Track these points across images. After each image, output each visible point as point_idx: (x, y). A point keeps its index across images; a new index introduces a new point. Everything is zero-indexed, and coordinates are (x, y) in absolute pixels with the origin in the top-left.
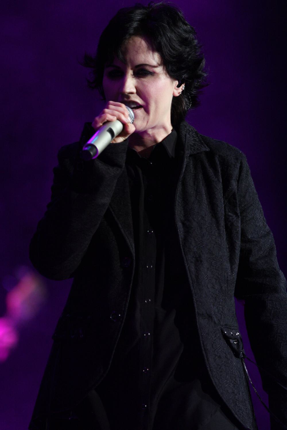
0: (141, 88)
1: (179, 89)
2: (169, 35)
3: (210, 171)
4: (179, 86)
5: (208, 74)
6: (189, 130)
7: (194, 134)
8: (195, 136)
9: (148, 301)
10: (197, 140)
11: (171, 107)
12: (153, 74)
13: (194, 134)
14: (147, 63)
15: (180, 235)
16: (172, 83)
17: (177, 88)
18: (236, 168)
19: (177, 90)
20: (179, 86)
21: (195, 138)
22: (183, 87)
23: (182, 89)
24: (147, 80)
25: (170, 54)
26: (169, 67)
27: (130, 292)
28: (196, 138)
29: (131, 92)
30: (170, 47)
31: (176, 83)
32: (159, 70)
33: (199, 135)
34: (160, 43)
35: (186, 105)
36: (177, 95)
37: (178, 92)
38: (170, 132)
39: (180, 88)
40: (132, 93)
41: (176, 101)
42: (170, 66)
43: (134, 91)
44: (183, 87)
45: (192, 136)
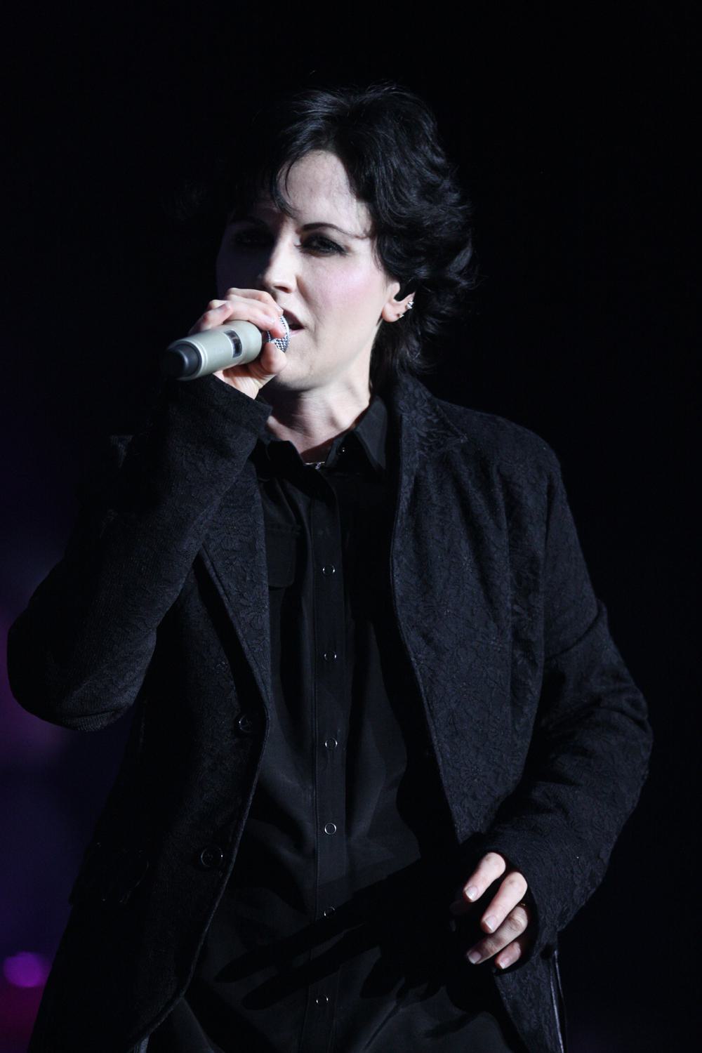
0: (309, 283)
1: (399, 305)
2: (395, 165)
3: (478, 501)
4: (399, 297)
5: (474, 282)
6: (415, 398)
7: (426, 405)
8: (428, 411)
9: (331, 743)
10: (435, 421)
11: (373, 346)
12: (340, 250)
13: (426, 405)
14: (334, 223)
15: (417, 669)
16: (385, 285)
17: (394, 301)
18: (429, 636)
19: (393, 305)
20: (399, 297)
21: (429, 418)
22: (409, 301)
23: (406, 307)
24: (329, 265)
25: (391, 209)
26: (384, 243)
27: (251, 798)
28: (431, 415)
29: (283, 285)
30: (395, 195)
31: (396, 287)
32: (364, 251)
33: (438, 407)
34: (371, 179)
35: (411, 352)
36: (392, 317)
37: (397, 311)
38: (366, 404)
39: (402, 302)
40: (285, 289)
41: (388, 335)
42: (387, 241)
43: (292, 285)
44: (409, 301)
45: (421, 412)
